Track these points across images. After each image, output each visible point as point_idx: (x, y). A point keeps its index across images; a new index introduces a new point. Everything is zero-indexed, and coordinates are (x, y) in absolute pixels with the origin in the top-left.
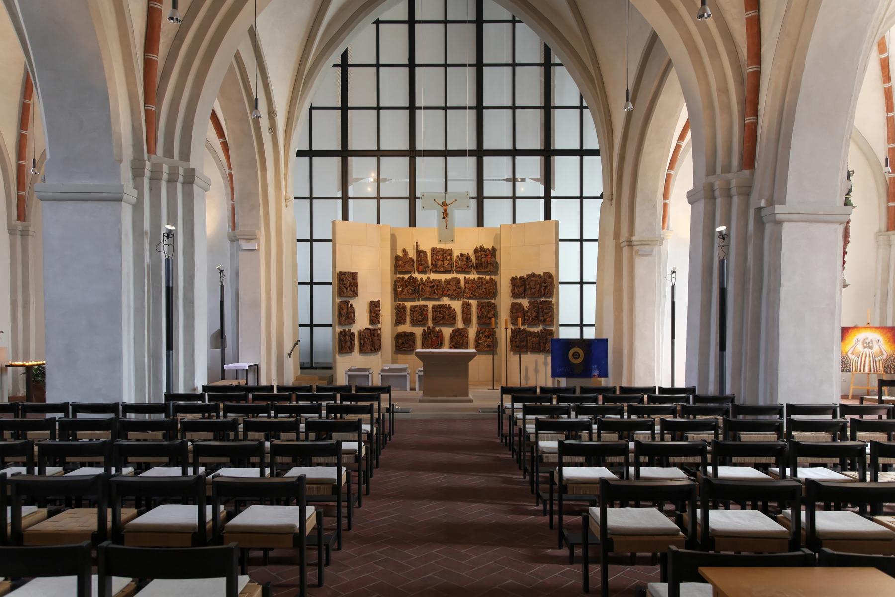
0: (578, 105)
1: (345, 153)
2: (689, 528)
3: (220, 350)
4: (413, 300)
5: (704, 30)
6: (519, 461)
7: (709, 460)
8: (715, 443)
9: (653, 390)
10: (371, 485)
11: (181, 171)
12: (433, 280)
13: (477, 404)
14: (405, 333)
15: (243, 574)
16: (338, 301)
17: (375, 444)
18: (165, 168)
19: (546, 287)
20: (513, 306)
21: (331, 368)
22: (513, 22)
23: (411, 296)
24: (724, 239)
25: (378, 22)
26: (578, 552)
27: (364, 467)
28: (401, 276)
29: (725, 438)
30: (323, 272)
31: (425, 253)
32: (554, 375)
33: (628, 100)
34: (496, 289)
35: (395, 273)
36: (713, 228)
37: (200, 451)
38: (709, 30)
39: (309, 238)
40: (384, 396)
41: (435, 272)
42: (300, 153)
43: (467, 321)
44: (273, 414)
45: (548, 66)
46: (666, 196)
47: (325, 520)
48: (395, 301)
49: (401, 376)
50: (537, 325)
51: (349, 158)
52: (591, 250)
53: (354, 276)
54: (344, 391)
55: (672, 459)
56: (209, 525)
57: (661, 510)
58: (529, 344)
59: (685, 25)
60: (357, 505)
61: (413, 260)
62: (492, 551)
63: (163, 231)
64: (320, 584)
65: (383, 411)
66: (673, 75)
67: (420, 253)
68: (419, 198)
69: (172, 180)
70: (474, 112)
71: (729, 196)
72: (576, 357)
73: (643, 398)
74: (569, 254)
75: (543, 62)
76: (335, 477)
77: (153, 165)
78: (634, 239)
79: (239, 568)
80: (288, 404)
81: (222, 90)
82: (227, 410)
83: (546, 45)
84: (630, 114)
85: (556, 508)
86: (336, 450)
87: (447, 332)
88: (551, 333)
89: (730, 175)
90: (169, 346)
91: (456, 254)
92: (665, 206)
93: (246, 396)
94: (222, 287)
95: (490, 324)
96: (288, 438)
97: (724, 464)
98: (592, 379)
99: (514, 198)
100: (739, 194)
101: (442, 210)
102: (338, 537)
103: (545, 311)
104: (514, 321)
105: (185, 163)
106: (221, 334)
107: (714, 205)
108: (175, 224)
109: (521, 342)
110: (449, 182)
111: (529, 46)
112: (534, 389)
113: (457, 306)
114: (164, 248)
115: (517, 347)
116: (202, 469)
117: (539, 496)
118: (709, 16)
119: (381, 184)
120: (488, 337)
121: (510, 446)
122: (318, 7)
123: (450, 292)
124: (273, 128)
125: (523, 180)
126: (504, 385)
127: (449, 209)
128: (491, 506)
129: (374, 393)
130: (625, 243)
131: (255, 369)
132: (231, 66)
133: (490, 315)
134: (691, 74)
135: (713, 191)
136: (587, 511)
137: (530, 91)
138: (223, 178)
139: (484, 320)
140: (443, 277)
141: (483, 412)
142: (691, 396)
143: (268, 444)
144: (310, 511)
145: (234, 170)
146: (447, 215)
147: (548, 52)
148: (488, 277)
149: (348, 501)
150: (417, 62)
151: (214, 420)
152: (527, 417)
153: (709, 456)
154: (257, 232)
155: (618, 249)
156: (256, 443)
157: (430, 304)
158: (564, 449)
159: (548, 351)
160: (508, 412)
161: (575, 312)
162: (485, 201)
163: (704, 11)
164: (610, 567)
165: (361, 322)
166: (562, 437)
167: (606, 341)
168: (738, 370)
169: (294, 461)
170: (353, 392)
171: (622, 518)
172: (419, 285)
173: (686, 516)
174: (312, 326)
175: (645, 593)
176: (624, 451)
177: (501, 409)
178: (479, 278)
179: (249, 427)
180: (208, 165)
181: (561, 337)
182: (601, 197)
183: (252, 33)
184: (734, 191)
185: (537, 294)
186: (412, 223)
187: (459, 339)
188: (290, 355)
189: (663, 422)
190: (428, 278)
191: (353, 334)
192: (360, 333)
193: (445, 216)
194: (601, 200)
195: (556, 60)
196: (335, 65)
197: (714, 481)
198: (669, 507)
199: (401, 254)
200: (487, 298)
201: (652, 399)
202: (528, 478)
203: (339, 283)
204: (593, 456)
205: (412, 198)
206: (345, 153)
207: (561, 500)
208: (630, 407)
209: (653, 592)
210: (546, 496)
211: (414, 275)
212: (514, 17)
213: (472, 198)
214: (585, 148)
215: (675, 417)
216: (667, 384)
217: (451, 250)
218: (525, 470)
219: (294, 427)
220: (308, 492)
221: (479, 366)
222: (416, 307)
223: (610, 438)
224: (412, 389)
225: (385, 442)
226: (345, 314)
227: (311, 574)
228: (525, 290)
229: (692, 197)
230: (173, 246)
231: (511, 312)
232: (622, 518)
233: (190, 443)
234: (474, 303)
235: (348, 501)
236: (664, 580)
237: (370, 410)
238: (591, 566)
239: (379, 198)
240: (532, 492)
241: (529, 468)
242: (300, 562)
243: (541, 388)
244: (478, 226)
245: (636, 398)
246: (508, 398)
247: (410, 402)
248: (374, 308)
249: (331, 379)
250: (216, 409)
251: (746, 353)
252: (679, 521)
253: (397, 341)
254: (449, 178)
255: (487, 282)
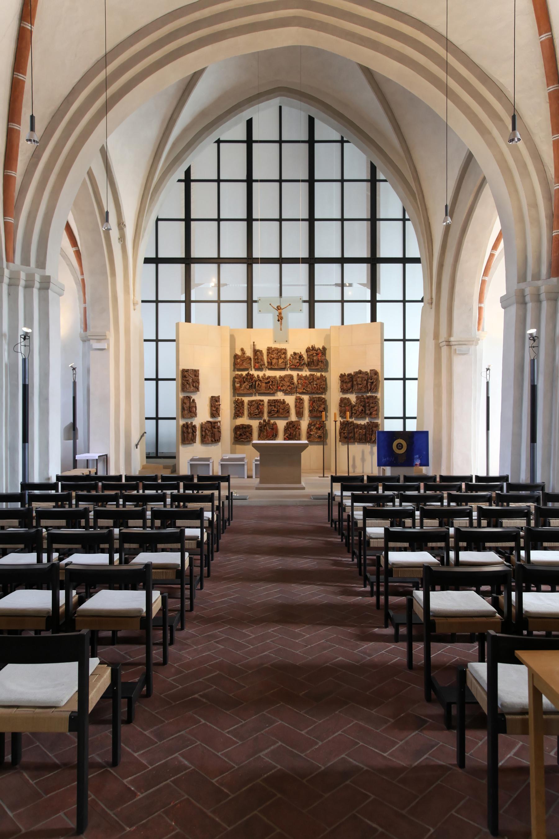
0: (401, 217)
1: (188, 261)
2: (505, 610)
3: (72, 441)
4: (250, 395)
5: (516, 153)
6: (347, 544)
7: (522, 544)
8: (528, 530)
9: (470, 478)
10: (211, 568)
11: (37, 278)
12: (269, 377)
13: (310, 491)
14: (242, 425)
15: (93, 656)
16: (181, 396)
17: (216, 529)
18: (23, 276)
19: (372, 383)
20: (342, 400)
21: (174, 457)
22: (342, 142)
23: (249, 392)
24: (534, 341)
25: (219, 142)
26: (403, 630)
27: (205, 552)
28: (240, 373)
29: (537, 525)
30: (168, 369)
31: (261, 352)
32: (379, 465)
33: (446, 215)
34: (326, 384)
35: (234, 371)
36: (524, 330)
37: (54, 538)
38: (519, 151)
39: (155, 343)
40: (224, 484)
41: (270, 369)
42: (147, 261)
43: (300, 414)
44: (121, 501)
45: (373, 181)
46: (481, 300)
47: (170, 601)
48: (234, 396)
49: (239, 465)
50: (363, 418)
51: (192, 265)
52: (413, 349)
53: (196, 373)
54: (187, 479)
55: (488, 544)
56: (62, 609)
57: (478, 592)
58: (356, 435)
59: (498, 146)
60: (199, 587)
61: (250, 359)
62: (323, 630)
63: (20, 333)
64: (165, 662)
65: (223, 499)
66: (487, 191)
67: (256, 352)
68: (256, 302)
69: (29, 286)
70: (307, 223)
71: (539, 301)
72: (400, 448)
73: (460, 487)
74: (393, 351)
75: (369, 217)
76: (179, 562)
77: (11, 272)
78: (452, 339)
79: (90, 647)
80: (135, 492)
81: (76, 204)
82: (79, 498)
83: (372, 164)
84: (448, 228)
85: (382, 589)
86: (180, 537)
87: (281, 424)
88: (377, 425)
89: (539, 283)
90: (25, 439)
91: (290, 353)
92: (480, 309)
93: (96, 485)
94: (75, 383)
95: (321, 417)
96: (135, 527)
97: (535, 549)
98: (414, 468)
99: (342, 301)
100: (548, 299)
101: (277, 313)
102: (182, 619)
103: (370, 406)
104: (342, 414)
105: (40, 271)
106: (74, 426)
107: (525, 310)
108: (31, 327)
109: (349, 433)
110: (283, 287)
111: (357, 163)
112: (361, 479)
113: (290, 400)
114: (21, 349)
115: (345, 438)
116: (55, 555)
117: (366, 579)
118: (519, 140)
119: (221, 288)
120: (319, 429)
121: (339, 531)
122: (162, 132)
123: (284, 388)
124: (122, 238)
125: (350, 285)
126: (334, 475)
127: (284, 312)
128: (322, 588)
129: (214, 482)
130: (444, 343)
131: (105, 459)
132: (84, 182)
133: (321, 409)
134: (504, 189)
135: (524, 296)
136: (411, 593)
137: (357, 202)
138: (76, 283)
139: (315, 414)
140: (278, 374)
141: (314, 499)
142: (505, 484)
143: (116, 531)
144: (156, 595)
145: (86, 277)
146: (282, 318)
147: (373, 169)
148: (319, 374)
149: (191, 584)
150: (254, 178)
151: (67, 508)
152: (355, 504)
153: (522, 540)
154: (107, 333)
155: (438, 348)
156: (105, 531)
157: (266, 399)
158: (389, 536)
159: (374, 442)
160: (338, 499)
161: (397, 408)
162: (316, 304)
163: (515, 135)
164: (433, 645)
165: (203, 415)
166: (387, 523)
167: (427, 433)
168: (547, 460)
169: (140, 547)
170: (196, 481)
171: (444, 601)
172: (256, 381)
173: (502, 598)
174: (157, 419)
175: (465, 672)
176: (445, 537)
177: (331, 497)
178: (311, 375)
179: (99, 515)
180: (61, 269)
181: (386, 429)
182: (422, 301)
183: (104, 152)
184: (543, 297)
185: (364, 390)
186: (250, 324)
187: (292, 431)
188: (137, 446)
189: (480, 509)
190: (264, 375)
191: (194, 427)
192: (202, 426)
193: (280, 319)
194: (422, 304)
195: (380, 176)
196: (179, 181)
197: (528, 567)
198: (486, 588)
199: (239, 353)
200: (317, 393)
201: (470, 488)
202: (356, 560)
203: (182, 379)
204: (417, 542)
205: (250, 302)
206: (188, 261)
207: (387, 582)
208: (449, 495)
209: (473, 672)
210: (373, 578)
211: (251, 373)
212: (342, 138)
213: (305, 302)
214: (407, 256)
215: (491, 505)
216: (483, 474)
217: (285, 350)
218: (354, 553)
219: (141, 515)
220: (154, 577)
221: (311, 455)
222: (252, 401)
223: (431, 524)
224: (250, 477)
225: (224, 527)
226: (188, 408)
227: (157, 653)
228: (352, 386)
229: (505, 302)
230: (29, 347)
231: (340, 406)
232: (444, 601)
233: (44, 530)
234: (306, 398)
235: (191, 584)
236: (482, 660)
237: (210, 499)
238: (415, 644)
239: (219, 302)
240: (360, 574)
241: (357, 551)
242: (146, 641)
243: (368, 477)
244: (310, 327)
245: (455, 486)
246: (337, 487)
247: (248, 489)
248: (215, 402)
249: (174, 468)
250: (68, 498)
251: (555, 446)
252: (495, 603)
253: (235, 433)
254: (283, 284)
255: (318, 379)
